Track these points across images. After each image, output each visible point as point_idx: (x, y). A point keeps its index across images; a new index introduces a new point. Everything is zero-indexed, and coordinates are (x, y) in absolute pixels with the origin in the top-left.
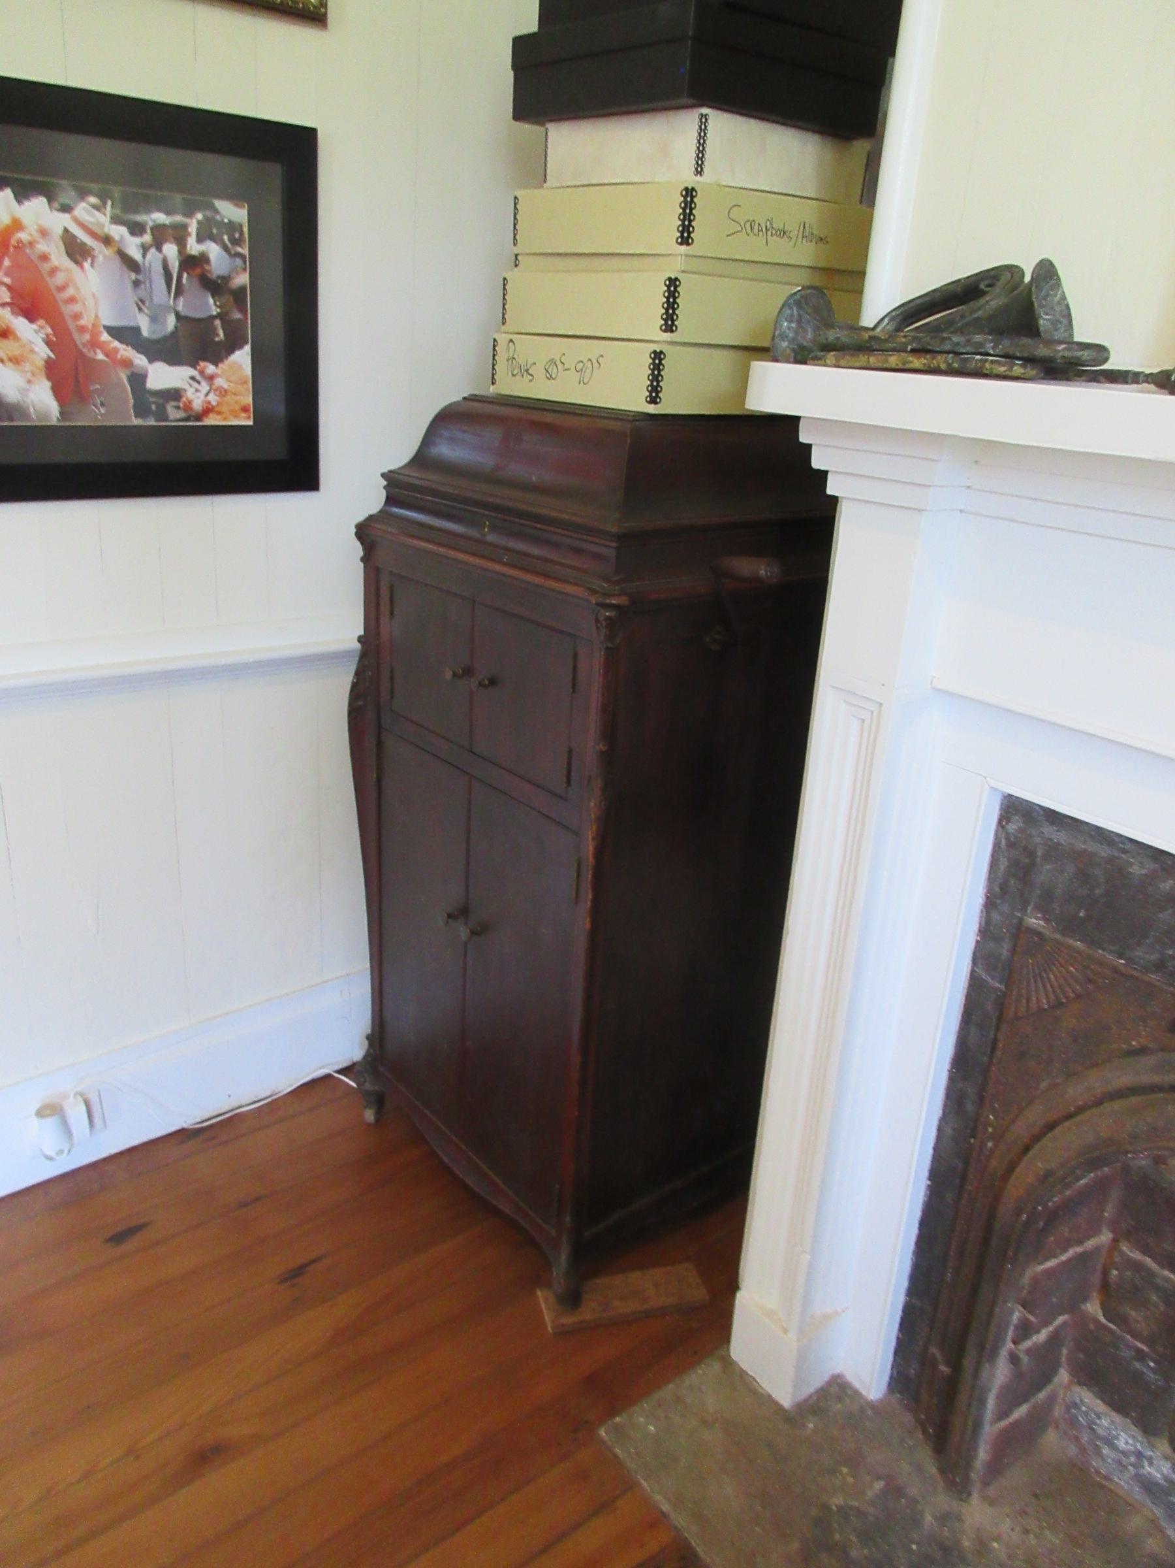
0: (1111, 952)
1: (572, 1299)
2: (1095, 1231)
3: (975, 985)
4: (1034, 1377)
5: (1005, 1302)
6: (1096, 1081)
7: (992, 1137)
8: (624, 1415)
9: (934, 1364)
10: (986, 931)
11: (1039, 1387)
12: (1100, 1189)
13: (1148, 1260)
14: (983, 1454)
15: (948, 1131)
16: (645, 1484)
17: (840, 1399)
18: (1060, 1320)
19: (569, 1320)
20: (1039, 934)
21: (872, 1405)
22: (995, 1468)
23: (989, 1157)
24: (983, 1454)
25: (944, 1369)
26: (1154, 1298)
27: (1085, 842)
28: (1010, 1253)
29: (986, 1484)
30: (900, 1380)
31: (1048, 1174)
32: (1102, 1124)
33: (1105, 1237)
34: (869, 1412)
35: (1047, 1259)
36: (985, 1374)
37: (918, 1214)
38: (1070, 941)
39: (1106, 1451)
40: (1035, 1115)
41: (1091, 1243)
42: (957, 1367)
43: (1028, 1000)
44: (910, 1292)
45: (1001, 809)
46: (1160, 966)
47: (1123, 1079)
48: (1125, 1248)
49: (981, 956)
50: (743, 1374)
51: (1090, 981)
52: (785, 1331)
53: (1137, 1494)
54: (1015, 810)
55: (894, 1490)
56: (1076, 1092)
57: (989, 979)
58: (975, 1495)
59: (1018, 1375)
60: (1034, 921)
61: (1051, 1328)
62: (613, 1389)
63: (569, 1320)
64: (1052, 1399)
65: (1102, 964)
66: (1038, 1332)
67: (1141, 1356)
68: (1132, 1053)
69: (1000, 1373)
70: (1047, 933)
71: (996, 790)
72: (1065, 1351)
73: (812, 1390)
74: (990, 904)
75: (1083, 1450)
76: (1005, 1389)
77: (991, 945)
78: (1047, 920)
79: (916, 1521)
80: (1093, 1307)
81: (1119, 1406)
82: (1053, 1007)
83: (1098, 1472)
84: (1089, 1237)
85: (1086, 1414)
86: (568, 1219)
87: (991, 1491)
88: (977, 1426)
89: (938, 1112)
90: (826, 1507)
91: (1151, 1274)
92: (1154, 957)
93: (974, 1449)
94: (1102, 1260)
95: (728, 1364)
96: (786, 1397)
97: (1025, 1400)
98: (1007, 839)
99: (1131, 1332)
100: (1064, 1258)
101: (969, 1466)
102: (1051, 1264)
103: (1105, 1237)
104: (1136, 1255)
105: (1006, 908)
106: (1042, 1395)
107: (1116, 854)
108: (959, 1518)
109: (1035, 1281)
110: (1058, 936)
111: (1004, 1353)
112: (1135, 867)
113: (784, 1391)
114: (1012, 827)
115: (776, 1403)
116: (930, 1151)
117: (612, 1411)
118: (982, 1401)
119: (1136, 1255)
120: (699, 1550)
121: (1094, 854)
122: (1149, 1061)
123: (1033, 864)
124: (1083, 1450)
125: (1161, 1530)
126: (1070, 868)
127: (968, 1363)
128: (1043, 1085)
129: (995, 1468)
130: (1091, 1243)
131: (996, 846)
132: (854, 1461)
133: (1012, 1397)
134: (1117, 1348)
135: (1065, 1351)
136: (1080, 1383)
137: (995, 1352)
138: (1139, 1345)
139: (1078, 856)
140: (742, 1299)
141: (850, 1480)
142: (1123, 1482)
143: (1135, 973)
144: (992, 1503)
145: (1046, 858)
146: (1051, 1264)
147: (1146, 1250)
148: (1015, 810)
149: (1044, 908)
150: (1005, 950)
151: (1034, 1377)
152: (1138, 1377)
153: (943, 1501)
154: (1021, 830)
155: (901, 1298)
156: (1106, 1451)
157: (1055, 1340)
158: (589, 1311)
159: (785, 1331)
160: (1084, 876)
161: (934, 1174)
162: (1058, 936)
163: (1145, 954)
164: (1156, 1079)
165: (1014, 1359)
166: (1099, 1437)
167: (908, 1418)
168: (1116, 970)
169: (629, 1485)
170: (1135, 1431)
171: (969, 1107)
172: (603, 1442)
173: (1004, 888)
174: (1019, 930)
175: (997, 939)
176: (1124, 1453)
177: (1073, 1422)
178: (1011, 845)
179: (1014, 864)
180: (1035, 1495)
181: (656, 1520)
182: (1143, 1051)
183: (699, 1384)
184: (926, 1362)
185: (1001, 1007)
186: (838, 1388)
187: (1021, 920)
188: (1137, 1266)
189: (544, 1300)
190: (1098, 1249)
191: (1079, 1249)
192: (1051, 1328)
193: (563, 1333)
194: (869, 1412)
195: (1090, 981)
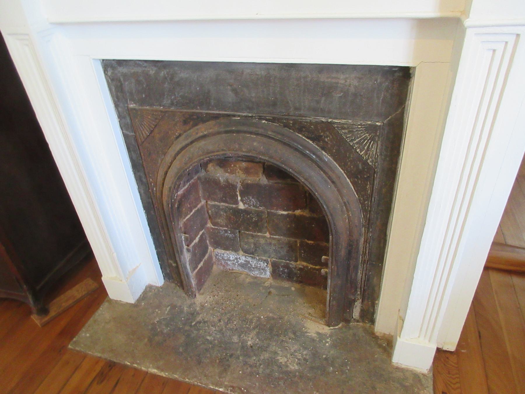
0: (157, 105)
1: (44, 311)
2: (198, 200)
3: (126, 136)
4: (200, 251)
5: (177, 235)
6: (172, 152)
7: (154, 187)
8: (77, 337)
9: (171, 264)
10: (120, 117)
11: (204, 255)
12: (194, 188)
13: (216, 203)
14: (193, 282)
15: (142, 192)
16: (90, 353)
17: (150, 291)
18: (201, 233)
19: (46, 319)
20: (134, 109)
21: (161, 287)
22: (200, 284)
23: (156, 193)
24: (193, 282)
25: (174, 265)
26: (222, 213)
27: (133, 69)
28: (172, 219)
29: (199, 290)
30: (167, 276)
31: (170, 188)
32: (176, 164)
33: (203, 202)
34: (161, 290)
35: (186, 216)
36: (182, 260)
37: (147, 223)
38: (145, 108)
39: (229, 263)
40: (161, 173)
41: (199, 206)
42: (176, 262)
43: (142, 134)
44: (156, 248)
45: (103, 68)
46: (172, 104)
47: (178, 148)
48: (209, 202)
49: (123, 126)
50: (116, 301)
51: (156, 119)
52: (121, 281)
53: (240, 269)
54: (110, 66)
55: (173, 307)
56: (168, 159)
57: (129, 133)
58: (197, 295)
59: (194, 255)
60: (132, 106)
61: (199, 236)
62: (70, 331)
63: (46, 319)
64: (210, 257)
65: (156, 111)
66: (195, 239)
67: (226, 231)
68: (177, 137)
69: (187, 257)
70: (137, 108)
71: (97, 59)
72: (208, 242)
73: (140, 293)
74: (117, 106)
75: (224, 266)
76: (191, 262)
77: (123, 120)
78: (135, 103)
79: (182, 311)
80: (209, 225)
81: (226, 248)
82: (151, 133)
83: (230, 269)
84: (198, 204)
85: (221, 256)
86: (25, 286)
87: (202, 291)
88: (187, 275)
89: (136, 187)
90: (153, 324)
91: (219, 206)
92: (169, 101)
93: (190, 282)
94: (206, 209)
95: (110, 301)
96: (132, 301)
97: (201, 261)
98: (110, 78)
99: (221, 226)
100: (191, 214)
101: (191, 286)
102: (189, 216)
103: (203, 202)
104: (213, 203)
105: (121, 105)
106: (206, 257)
107: (144, 69)
108: (195, 303)
109: (185, 224)
110: (140, 107)
111: (185, 250)
112: (151, 71)
113: (131, 299)
114: (109, 73)
115: (130, 304)
116: (140, 201)
117: (72, 338)
118: (186, 268)
119: (213, 203)
120: (115, 360)
121: (137, 72)
122: (183, 137)
123: (122, 85)
124: (224, 266)
125: (249, 275)
126: (133, 81)
127: (178, 259)
128: (160, 161)
129: (200, 284)
130: (199, 206)
131: (108, 82)
132: (159, 307)
133: (195, 262)
134: (220, 233)
135: (208, 242)
136: (216, 248)
137: (182, 251)
138: (224, 228)
139: (135, 75)
140: (105, 279)
141: (159, 312)
142: (237, 268)
143: (167, 110)
144: (203, 294)
145: (125, 81)
146: (189, 216)
147: (215, 200)
148: (110, 66)
149: (132, 100)
150: (128, 120)
151: (200, 251)
152: (227, 237)
153: (189, 302)
154: (112, 73)
155: (155, 252)
156: (229, 263)
157: (202, 239)
158: (53, 313)
159: (121, 281)
160: (138, 82)
161: (145, 208)
162: (140, 107)
163: (167, 102)
164: (187, 142)
165: (188, 250)
166: (226, 260)
167: (173, 285)
168: (161, 111)
169: (85, 356)
170: (233, 253)
171: (144, 180)
172: (71, 349)
173: (117, 97)
174: (130, 111)
175: (124, 118)
176: (234, 261)
177: (218, 260)
178: (112, 80)
179: (116, 87)
180: (215, 285)
181: (98, 360)
182: (180, 135)
183: (103, 313)
184: (170, 266)
185: (136, 141)
186: (150, 288)
187: (128, 107)
188: (214, 206)
189: (36, 319)
190: (202, 207)
191: (196, 209)
192: (199, 236)
193: (45, 325)
194: (161, 290)
195: (156, 119)
